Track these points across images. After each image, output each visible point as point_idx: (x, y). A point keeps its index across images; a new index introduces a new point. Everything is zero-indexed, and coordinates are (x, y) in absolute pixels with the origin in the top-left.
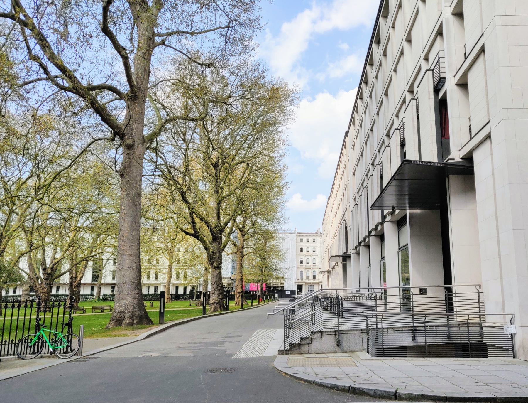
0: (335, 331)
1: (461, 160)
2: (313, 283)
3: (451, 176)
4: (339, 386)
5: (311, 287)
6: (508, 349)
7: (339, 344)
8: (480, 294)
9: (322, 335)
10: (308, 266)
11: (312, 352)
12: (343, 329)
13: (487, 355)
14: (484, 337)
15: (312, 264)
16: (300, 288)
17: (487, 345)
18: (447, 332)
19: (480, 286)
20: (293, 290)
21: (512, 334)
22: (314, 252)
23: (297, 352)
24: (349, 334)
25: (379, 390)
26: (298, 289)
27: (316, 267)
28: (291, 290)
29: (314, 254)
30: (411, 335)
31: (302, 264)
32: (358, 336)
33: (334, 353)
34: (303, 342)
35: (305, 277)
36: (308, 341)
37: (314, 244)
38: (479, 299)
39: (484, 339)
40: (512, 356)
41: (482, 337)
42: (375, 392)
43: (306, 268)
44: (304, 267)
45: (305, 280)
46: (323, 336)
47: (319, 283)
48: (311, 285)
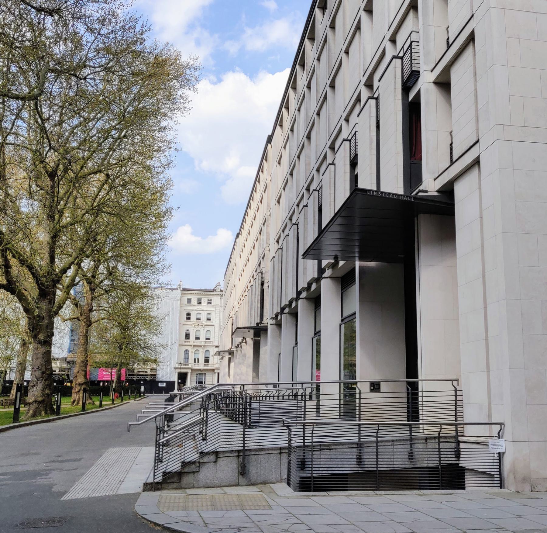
0: (239, 451)
1: (436, 194)
6: (494, 475)
7: (243, 471)
10: (198, 343)
13: (464, 485)
16: (183, 377)
19: (457, 380)
20: (172, 380)
21: (499, 453)
22: (209, 319)
23: (175, 485)
24: (260, 456)
26: (179, 379)
27: (211, 344)
28: (168, 380)
29: (209, 323)
31: (188, 338)
32: (274, 458)
33: (233, 486)
35: (191, 360)
36: (193, 468)
43: (194, 346)
44: (192, 343)
46: (219, 459)
48: (201, 373)
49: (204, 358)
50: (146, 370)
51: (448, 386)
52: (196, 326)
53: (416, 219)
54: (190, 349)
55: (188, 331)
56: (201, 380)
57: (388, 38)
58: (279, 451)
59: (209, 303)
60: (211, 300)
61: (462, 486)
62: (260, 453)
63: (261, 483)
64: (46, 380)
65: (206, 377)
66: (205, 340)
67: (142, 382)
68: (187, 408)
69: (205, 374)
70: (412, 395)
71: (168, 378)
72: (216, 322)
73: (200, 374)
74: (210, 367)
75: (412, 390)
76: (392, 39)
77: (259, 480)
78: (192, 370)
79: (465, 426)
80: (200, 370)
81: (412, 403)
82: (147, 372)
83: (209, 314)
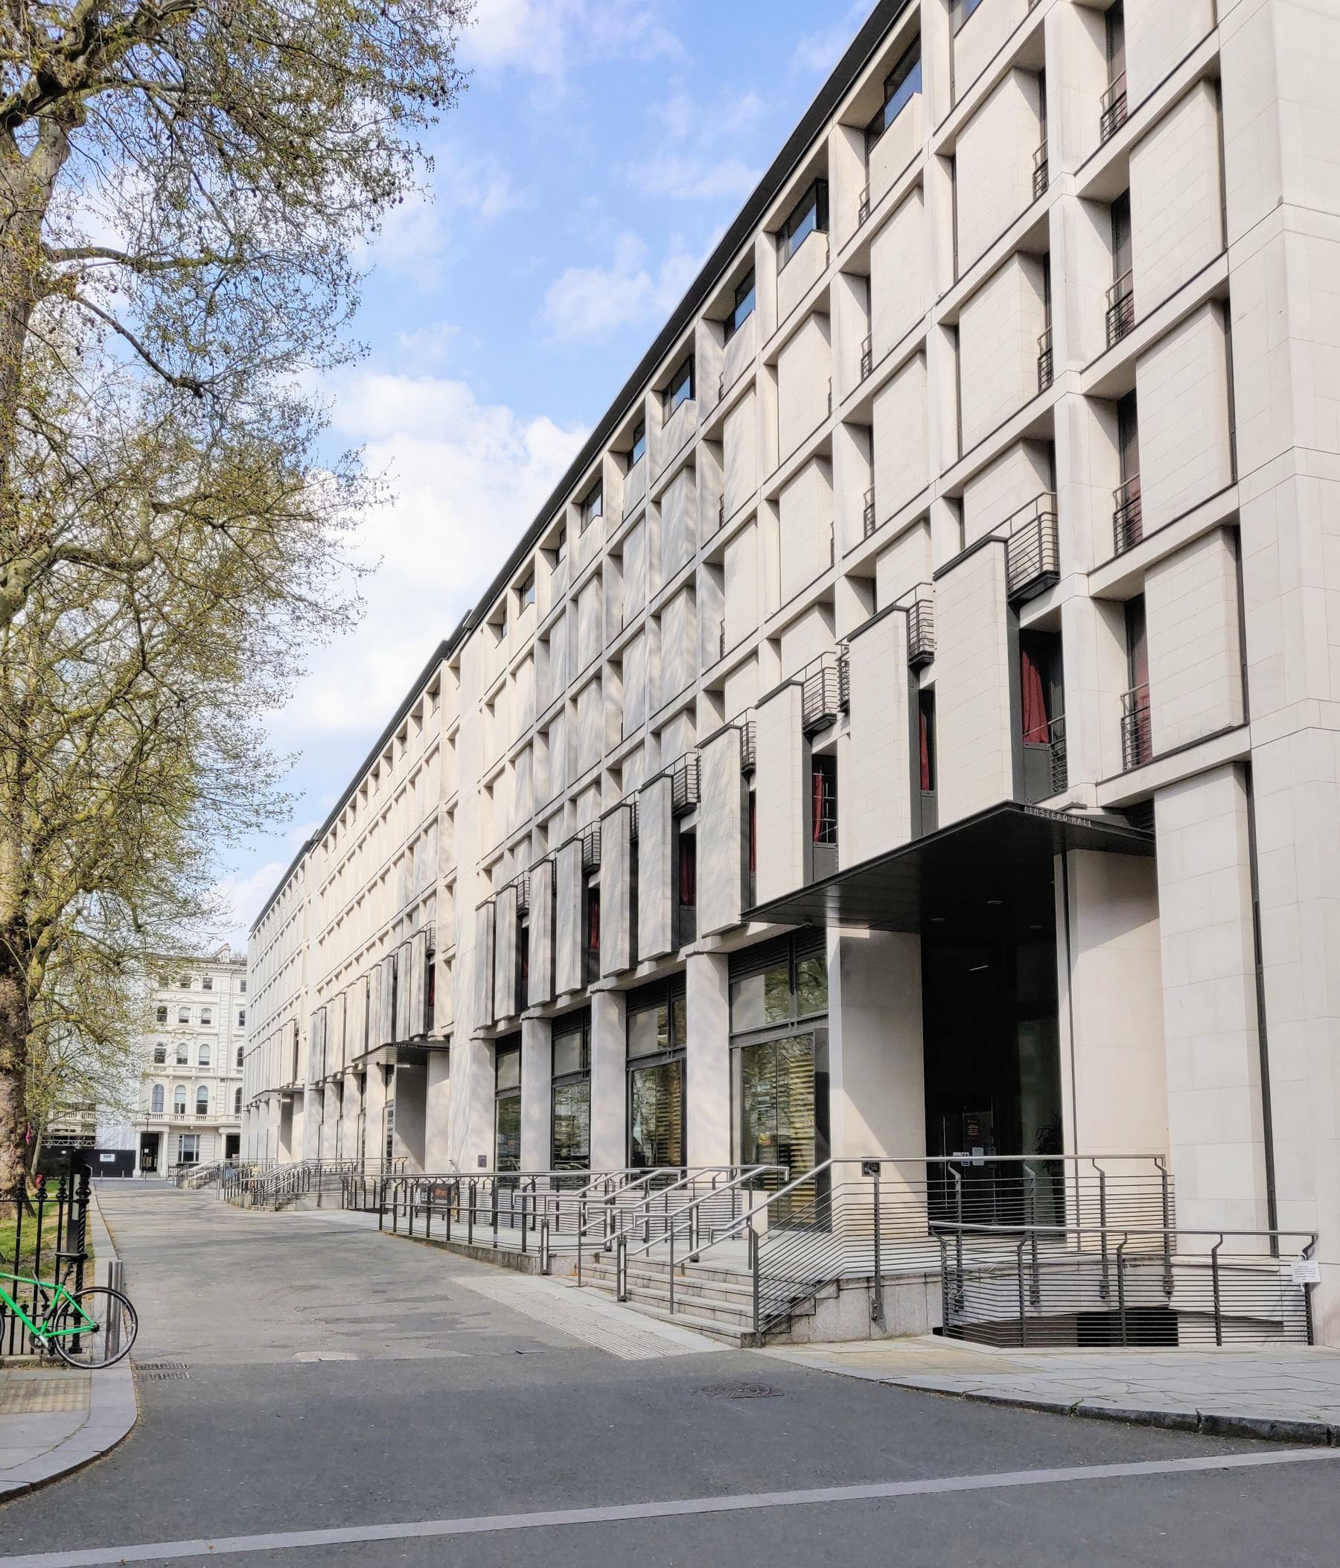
0: (868, 1279)
1: (1101, 812)
2: (196, 1128)
3: (1077, 852)
4: (1166, 1415)
5: (189, 1142)
6: (1281, 1322)
7: (877, 1314)
8: (1169, 1180)
9: (839, 1289)
10: (181, 1070)
11: (817, 1339)
12: (1095, 1267)
13: (1177, 1340)
14: (1175, 1294)
15: (197, 1065)
16: (151, 1142)
17: (1176, 1313)
18: (1101, 1278)
19: (1162, 1158)
20: (128, 1148)
21: (1306, 1285)
22: (206, 1022)
23: (784, 1337)
24: (897, 1288)
25: (1284, 1423)
26: (143, 1147)
27: (211, 1074)
28: (119, 1148)
29: (205, 1029)
30: (1098, 1283)
31: (162, 1061)
32: (917, 1290)
33: (863, 1339)
34: (798, 1311)
35: (169, 1107)
36: (807, 1307)
37: (207, 998)
38: (1102, 1196)
39: (1173, 1299)
40: (1215, 1340)
41: (1169, 1293)
42: (1273, 1427)
43: (176, 1077)
44: (170, 1072)
45: (168, 1115)
46: (841, 1293)
47: (216, 1129)
48: (190, 1134)
49: (195, 1104)
50: (72, 1127)
51: (1149, 1167)
52: (179, 1036)
53: (1058, 860)
54: (165, 1083)
55: (160, 1044)
56: (189, 1150)
57: (702, 436)
58: (923, 1280)
59: (208, 986)
60: (211, 980)
61: (1171, 1340)
62: (897, 1282)
63: (900, 1336)
64: (17, 1146)
65: (201, 1143)
66: (197, 1065)
67: (64, 1152)
68: (290, 1207)
69: (198, 1136)
70: (962, 1188)
71: (120, 1144)
72: (222, 1028)
73: (186, 1136)
74: (209, 1121)
75: (962, 1178)
76: (714, 438)
77: (900, 1330)
78: (171, 1127)
79: (1178, 1235)
80: (188, 1128)
81: (963, 1202)
82: (74, 1131)
83: (206, 1010)
